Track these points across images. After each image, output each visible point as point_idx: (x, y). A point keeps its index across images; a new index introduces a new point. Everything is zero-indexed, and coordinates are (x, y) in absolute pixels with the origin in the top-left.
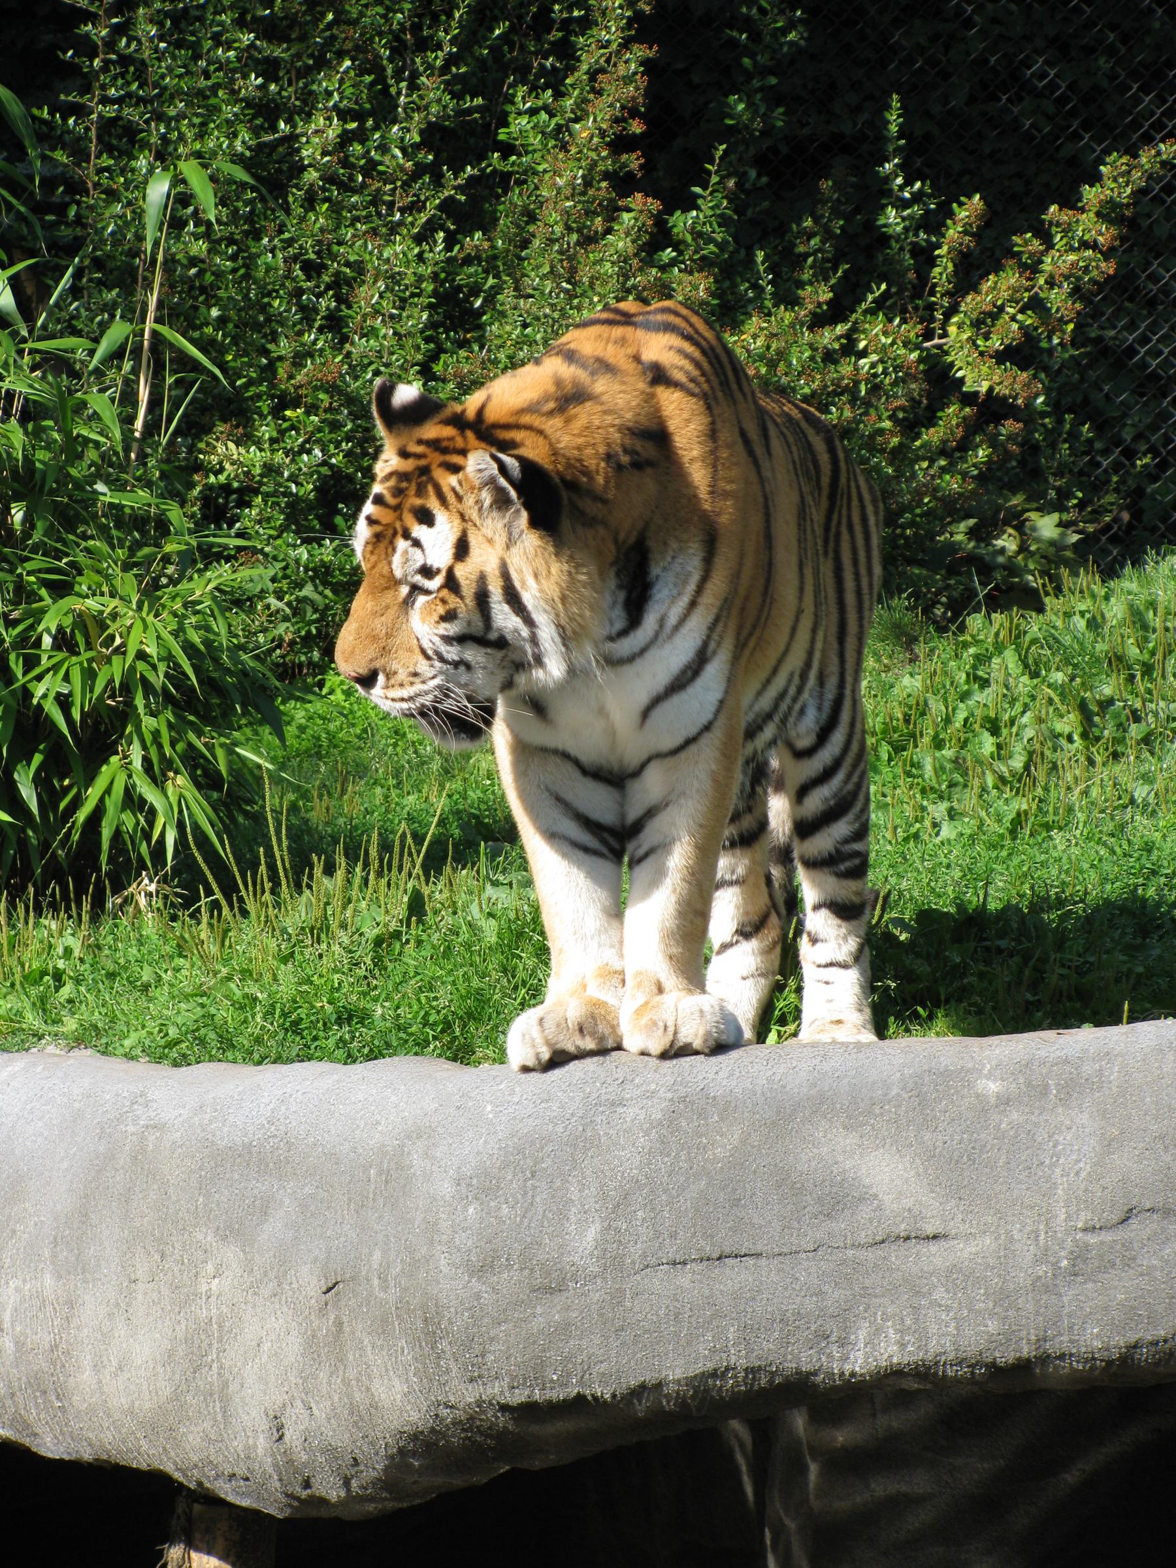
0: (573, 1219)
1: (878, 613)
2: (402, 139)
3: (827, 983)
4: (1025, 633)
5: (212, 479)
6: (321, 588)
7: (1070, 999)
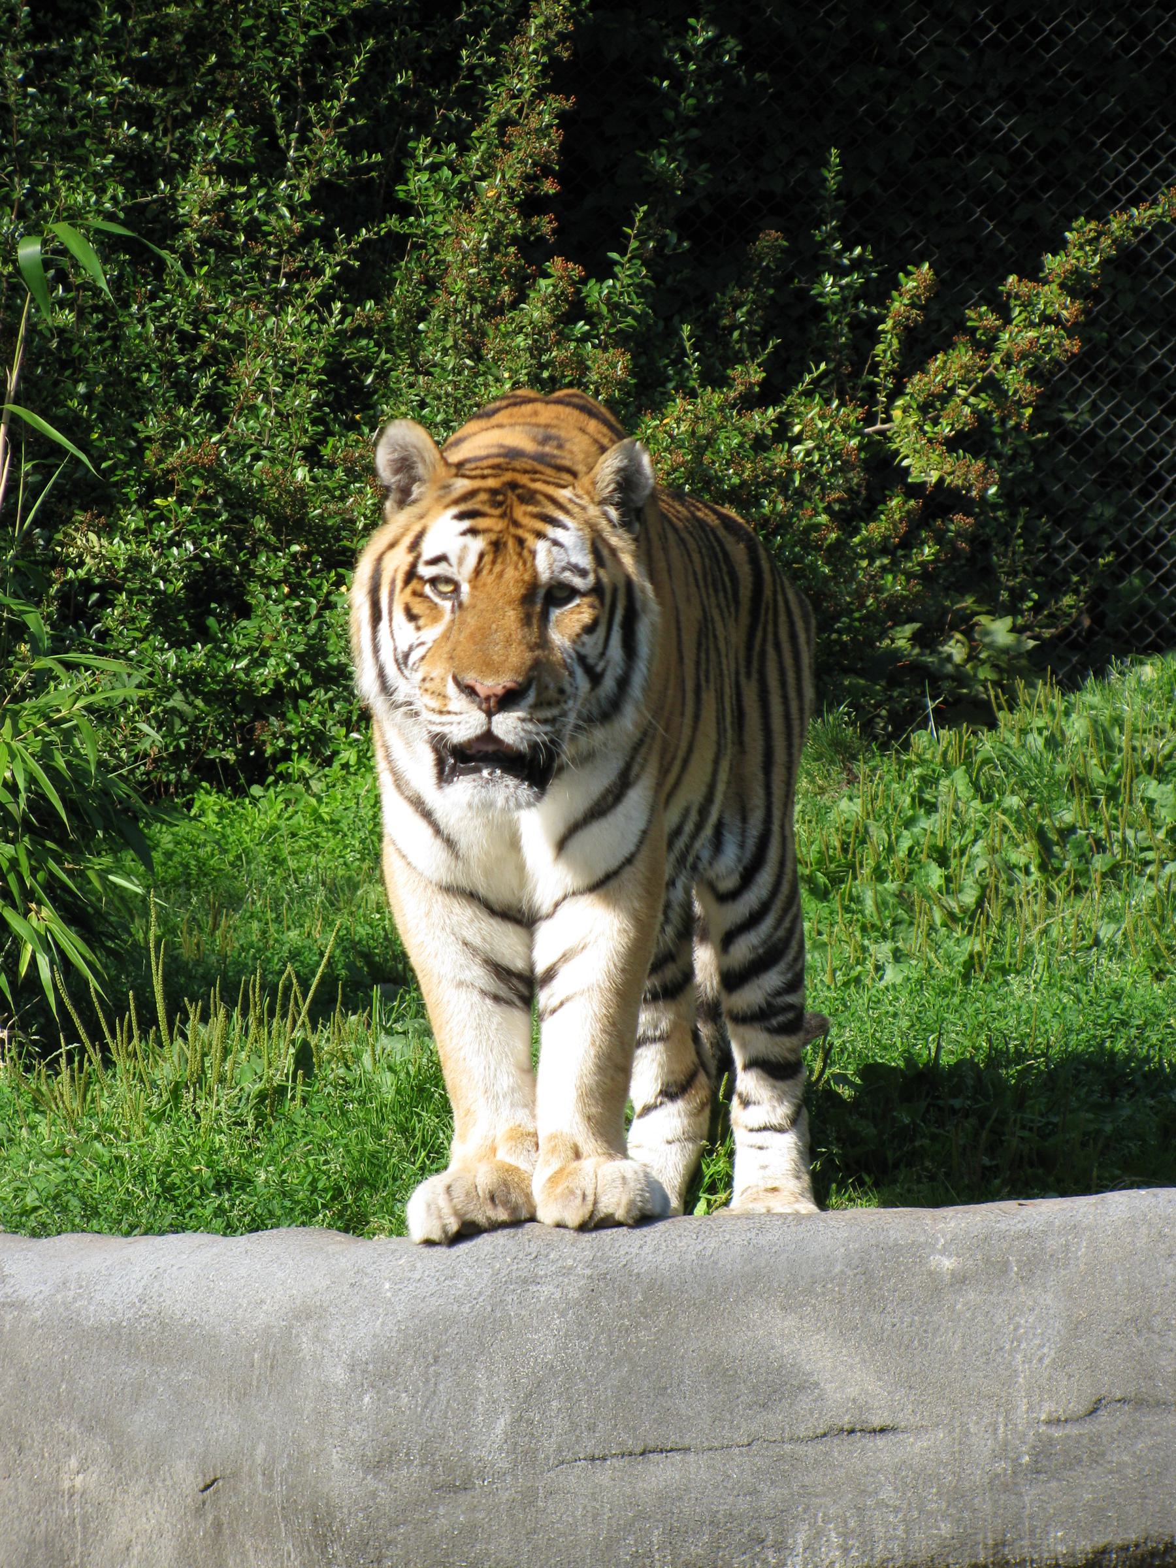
0: (480, 1409)
1: (814, 725)
2: (290, 197)
3: (761, 1148)
4: (977, 752)
5: (71, 574)
6: (192, 698)
7: (1032, 1165)
